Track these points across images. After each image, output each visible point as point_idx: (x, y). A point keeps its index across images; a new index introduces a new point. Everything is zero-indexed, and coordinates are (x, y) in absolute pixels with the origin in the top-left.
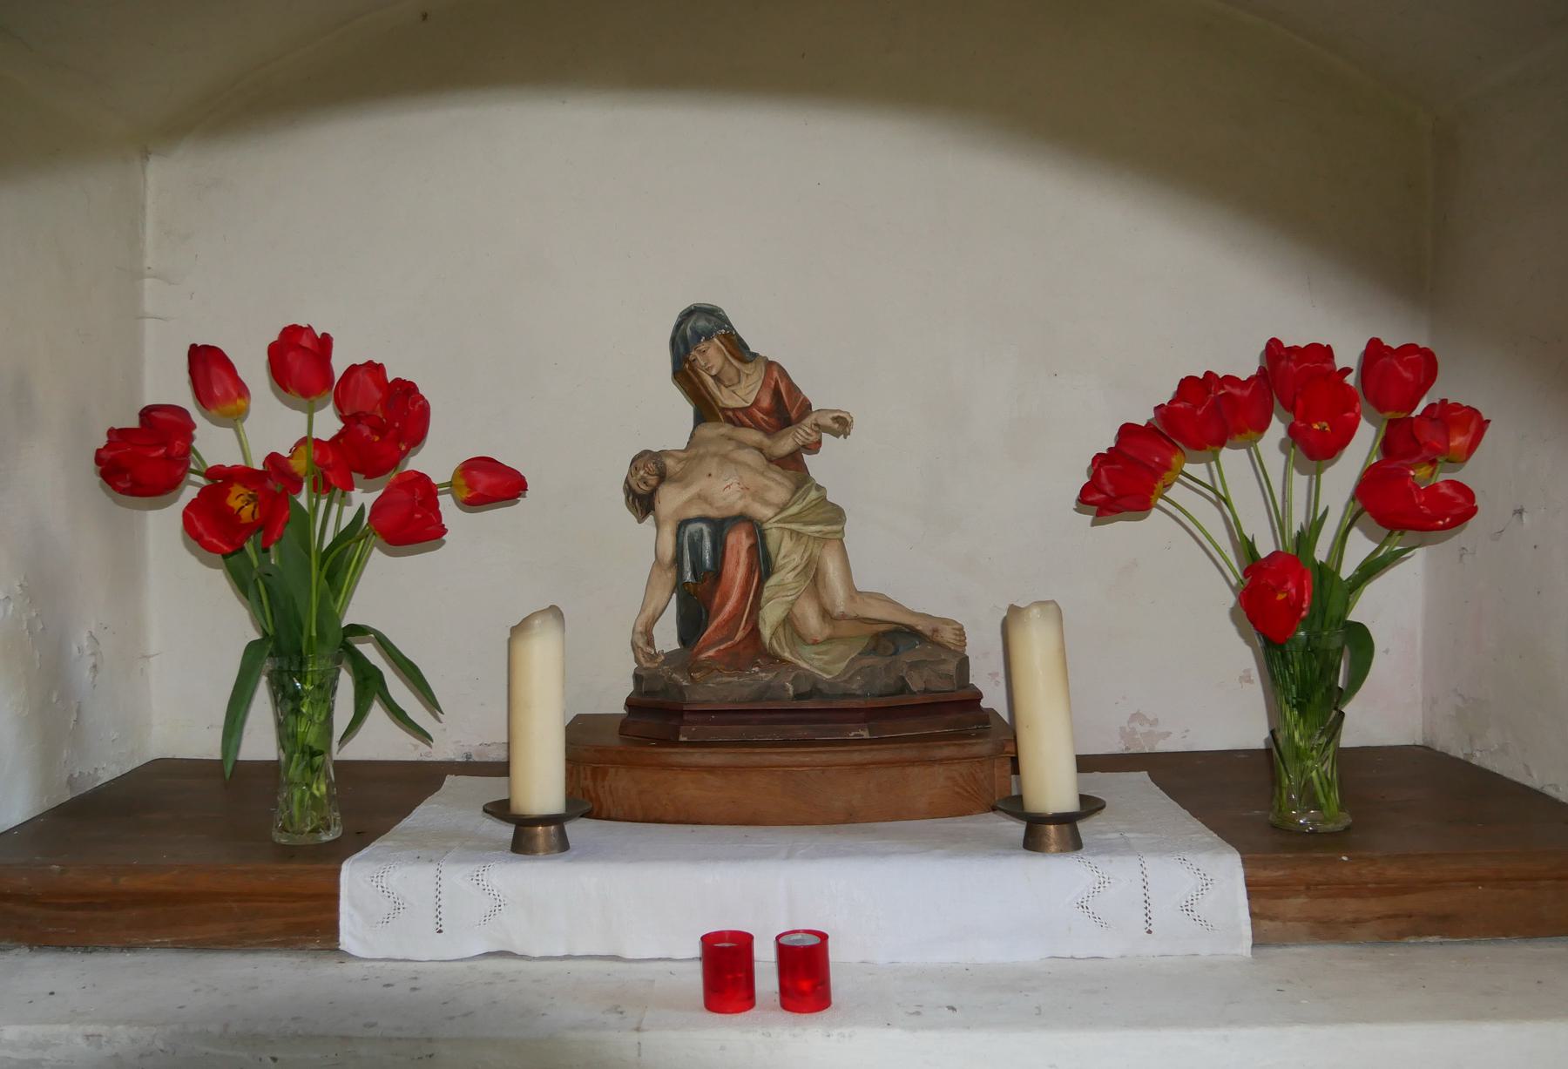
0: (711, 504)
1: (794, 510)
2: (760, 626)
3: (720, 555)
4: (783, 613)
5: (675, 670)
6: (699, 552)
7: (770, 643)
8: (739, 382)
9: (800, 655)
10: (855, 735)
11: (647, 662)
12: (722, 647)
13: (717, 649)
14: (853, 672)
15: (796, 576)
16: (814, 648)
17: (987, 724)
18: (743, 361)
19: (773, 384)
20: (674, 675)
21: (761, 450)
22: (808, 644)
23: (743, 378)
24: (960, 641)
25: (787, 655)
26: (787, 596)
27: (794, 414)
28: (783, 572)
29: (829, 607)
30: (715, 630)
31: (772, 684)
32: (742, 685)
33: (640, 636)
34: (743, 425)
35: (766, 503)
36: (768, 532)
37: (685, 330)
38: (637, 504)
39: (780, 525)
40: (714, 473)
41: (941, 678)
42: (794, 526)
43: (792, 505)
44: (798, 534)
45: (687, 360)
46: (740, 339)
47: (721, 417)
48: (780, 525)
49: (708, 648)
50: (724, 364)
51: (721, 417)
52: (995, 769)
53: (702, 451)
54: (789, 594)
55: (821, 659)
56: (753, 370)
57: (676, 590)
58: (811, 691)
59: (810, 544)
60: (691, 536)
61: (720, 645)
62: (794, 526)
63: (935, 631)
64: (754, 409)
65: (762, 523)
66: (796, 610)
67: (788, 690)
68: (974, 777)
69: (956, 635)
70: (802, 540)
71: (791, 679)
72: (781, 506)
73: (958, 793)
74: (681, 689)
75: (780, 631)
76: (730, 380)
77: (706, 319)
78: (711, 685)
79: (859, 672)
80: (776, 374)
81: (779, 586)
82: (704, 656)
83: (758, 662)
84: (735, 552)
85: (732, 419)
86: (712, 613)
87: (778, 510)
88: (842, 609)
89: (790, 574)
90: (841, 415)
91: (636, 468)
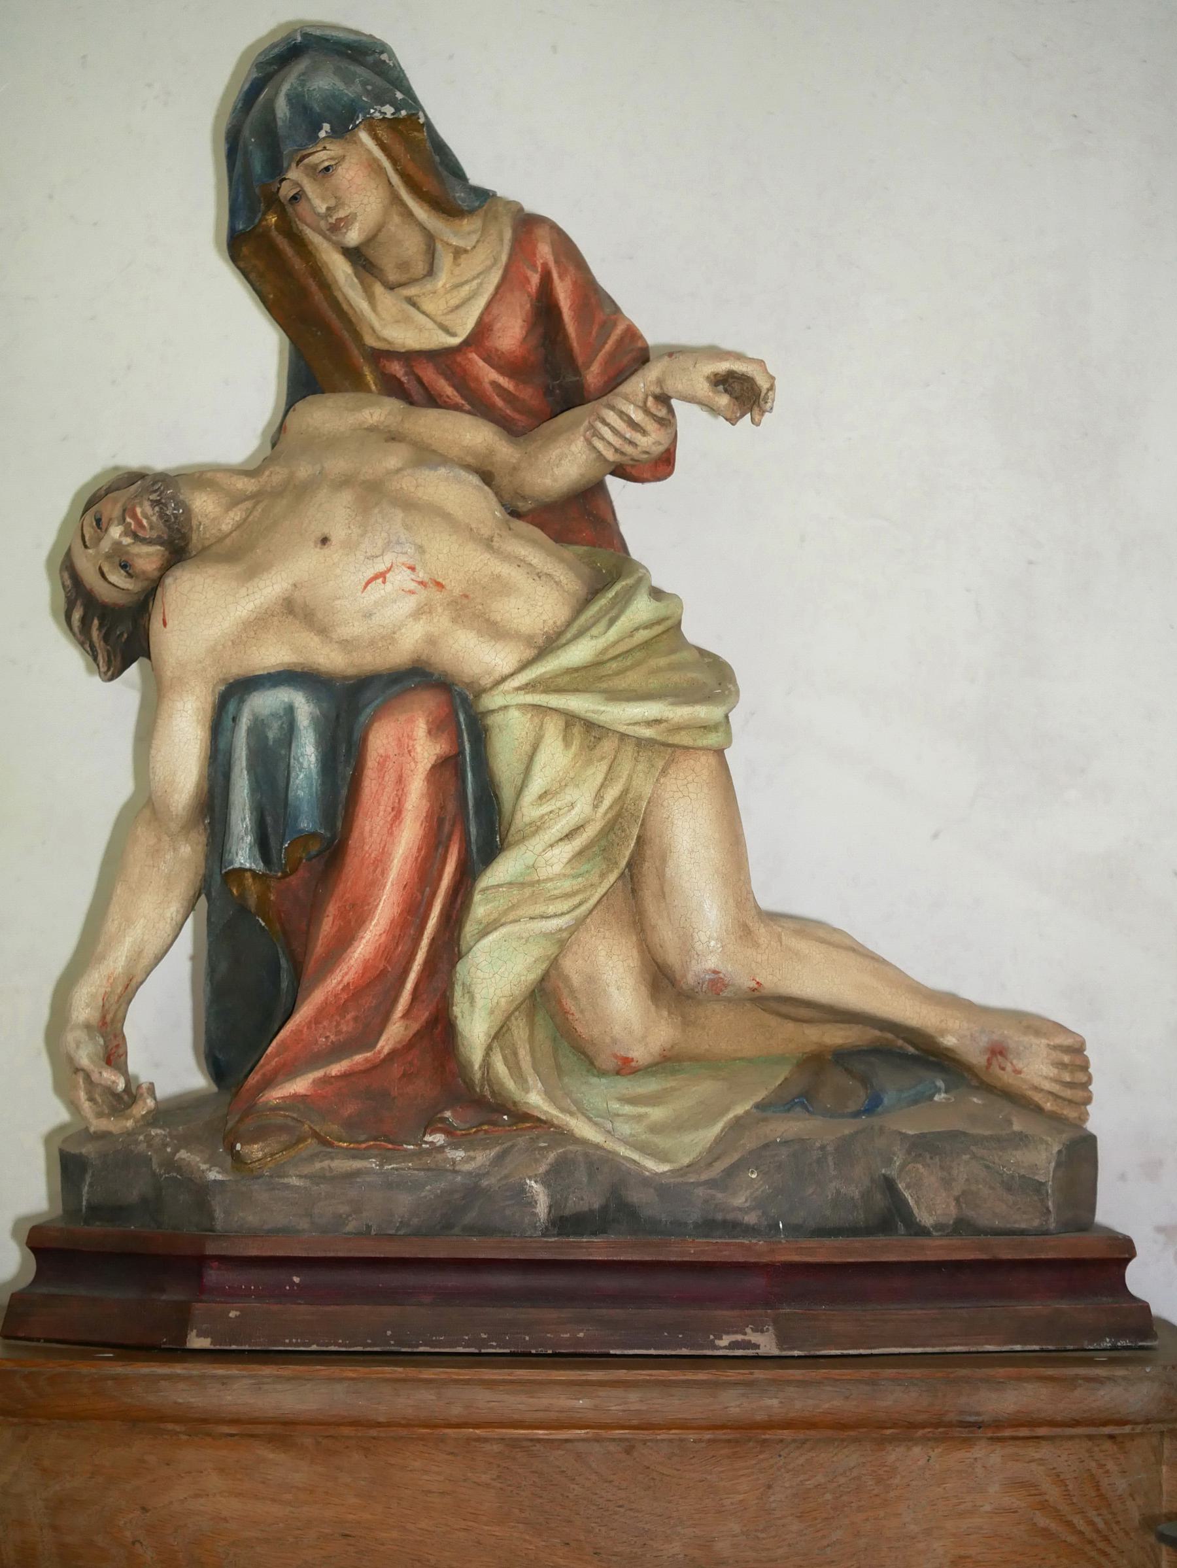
0: (323, 631)
1: (579, 653)
2: (457, 1010)
3: (344, 792)
4: (529, 970)
5: (185, 1141)
6: (282, 784)
7: (487, 1064)
8: (431, 272)
9: (575, 1102)
10: (734, 1345)
11: (100, 1115)
12: (336, 1069)
13: (319, 1074)
14: (736, 1157)
15: (580, 854)
16: (626, 1086)
17: (1145, 1339)
18: (447, 208)
19: (535, 279)
20: (183, 1154)
21: (487, 478)
22: (602, 1073)
23: (445, 260)
24: (1071, 1085)
25: (536, 1100)
26: (544, 917)
27: (593, 375)
28: (537, 844)
29: (673, 957)
30: (316, 1020)
31: (485, 1183)
32: (391, 1184)
33: (81, 1035)
34: (434, 401)
35: (495, 631)
36: (493, 720)
37: (270, 107)
38: (95, 634)
39: (531, 699)
40: (338, 533)
41: (1009, 1189)
42: (577, 703)
43: (576, 637)
44: (589, 726)
45: (273, 201)
46: (440, 147)
47: (370, 378)
48: (531, 699)
49: (290, 1070)
50: (386, 213)
51: (370, 378)
52: (1164, 1469)
53: (304, 471)
54: (551, 909)
55: (639, 1118)
56: (475, 238)
57: (203, 902)
58: (604, 1208)
59: (625, 767)
60: (258, 729)
61: (330, 1063)
62: (577, 703)
63: (998, 1051)
64: (474, 356)
65: (480, 692)
66: (572, 966)
67: (532, 1203)
68: (1097, 1487)
69: (1062, 1065)
70: (597, 752)
71: (542, 1169)
72: (540, 641)
73: (1046, 1533)
74: (202, 1192)
75: (519, 1031)
76: (404, 266)
77: (338, 71)
78: (294, 1181)
79: (753, 1159)
80: (545, 251)
81: (522, 885)
82: (277, 1094)
83: (444, 1120)
84: (390, 778)
85: (401, 383)
86: (311, 966)
87: (529, 653)
88: (712, 962)
89: (556, 851)
90: (739, 367)
91: (98, 521)
